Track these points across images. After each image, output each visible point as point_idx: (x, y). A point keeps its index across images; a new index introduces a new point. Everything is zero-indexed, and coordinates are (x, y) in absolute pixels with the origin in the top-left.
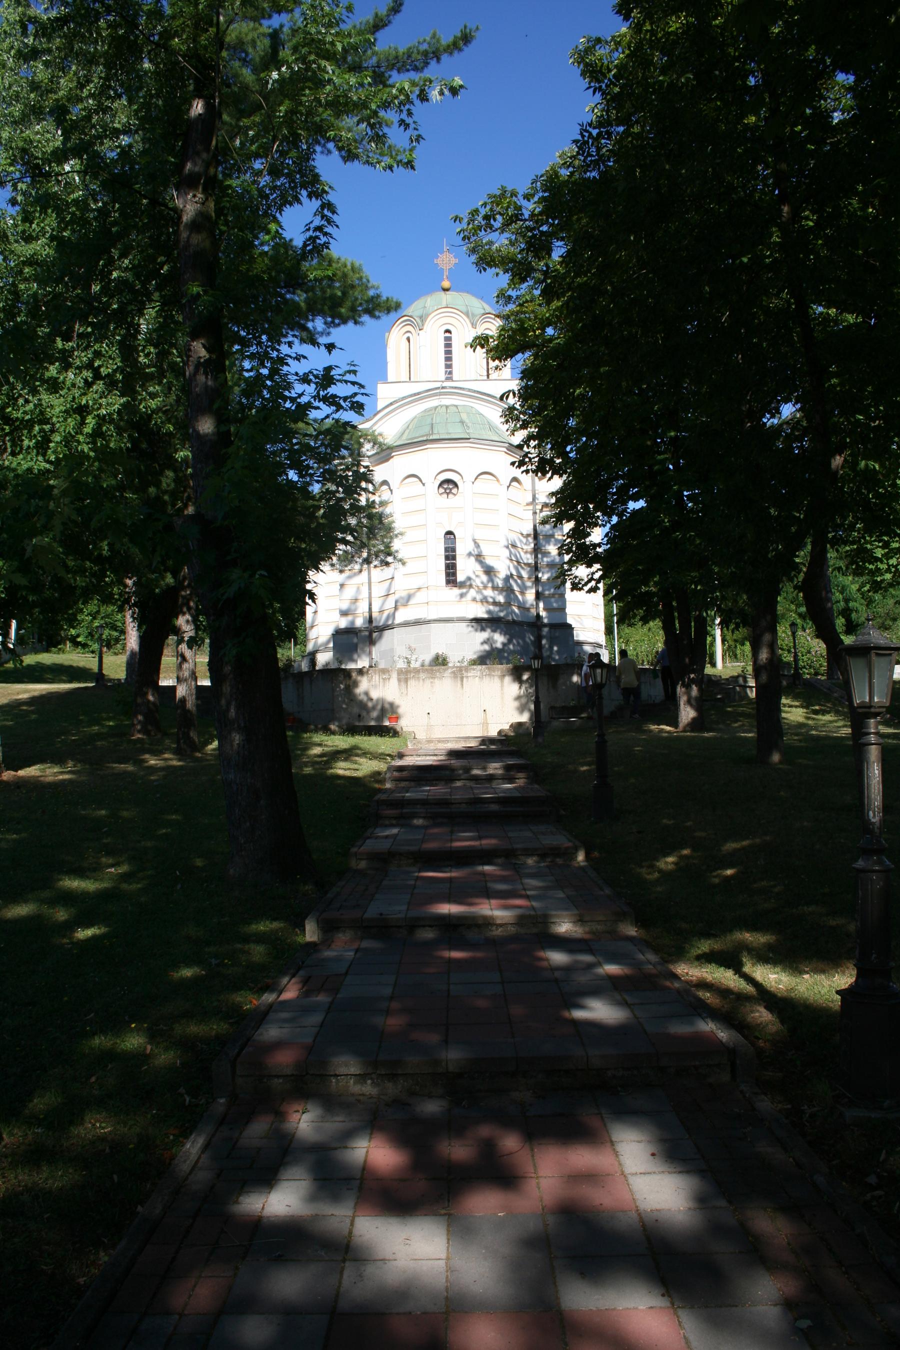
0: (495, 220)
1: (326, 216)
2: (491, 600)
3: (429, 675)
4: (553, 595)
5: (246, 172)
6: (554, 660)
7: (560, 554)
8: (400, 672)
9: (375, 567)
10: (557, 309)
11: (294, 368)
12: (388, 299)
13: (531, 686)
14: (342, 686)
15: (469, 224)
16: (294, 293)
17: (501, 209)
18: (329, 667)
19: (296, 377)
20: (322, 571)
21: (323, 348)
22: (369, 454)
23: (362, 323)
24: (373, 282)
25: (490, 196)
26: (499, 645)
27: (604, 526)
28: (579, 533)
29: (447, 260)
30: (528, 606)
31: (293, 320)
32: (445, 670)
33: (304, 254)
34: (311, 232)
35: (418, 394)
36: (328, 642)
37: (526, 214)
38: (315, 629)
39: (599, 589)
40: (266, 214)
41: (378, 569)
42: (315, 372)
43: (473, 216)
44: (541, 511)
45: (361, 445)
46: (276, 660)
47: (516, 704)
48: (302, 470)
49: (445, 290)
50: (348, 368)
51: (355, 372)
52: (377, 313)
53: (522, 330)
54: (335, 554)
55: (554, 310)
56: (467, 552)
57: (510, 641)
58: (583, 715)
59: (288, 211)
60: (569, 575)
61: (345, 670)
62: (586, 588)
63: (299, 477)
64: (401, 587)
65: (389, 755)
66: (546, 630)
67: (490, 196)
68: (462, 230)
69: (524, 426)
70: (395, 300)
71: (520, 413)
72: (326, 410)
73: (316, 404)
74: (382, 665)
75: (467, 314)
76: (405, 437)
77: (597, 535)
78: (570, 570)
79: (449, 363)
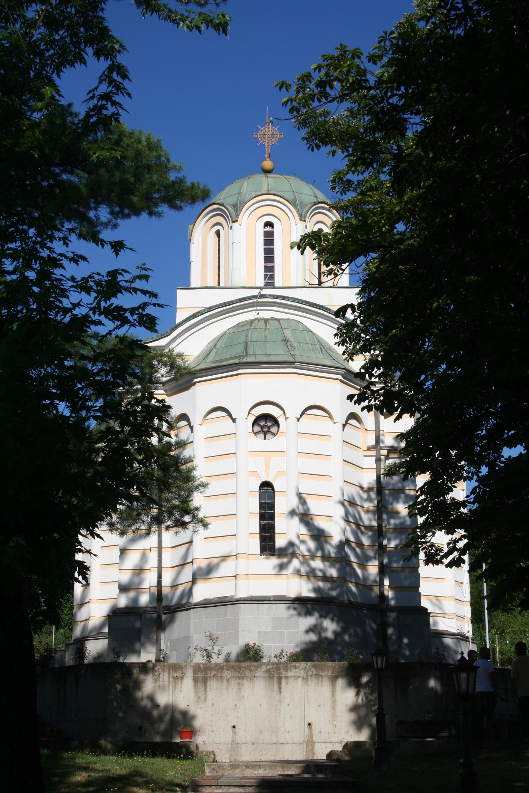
0: (332, 87)
1: (115, 81)
2: (320, 574)
3: (236, 674)
4: (403, 568)
5: (16, 20)
6: (404, 656)
7: (412, 515)
8: (197, 669)
9: (168, 528)
10: (410, 200)
11: (70, 270)
12: (193, 184)
13: (372, 692)
14: (119, 687)
15: (298, 93)
16: (72, 173)
17: (341, 71)
18: (101, 660)
19: (71, 283)
20: (98, 536)
21: (108, 247)
22: (164, 379)
23: (159, 215)
24: (174, 161)
25: (326, 58)
26: (329, 634)
27: (470, 479)
28: (436, 489)
29: (269, 135)
30: (369, 583)
31: (72, 209)
32: (257, 668)
33: (87, 127)
34: (95, 101)
35: (230, 303)
36: (102, 626)
37: (372, 80)
38: (85, 608)
39: (464, 562)
40: (39, 75)
41: (172, 531)
42: (97, 277)
43: (304, 82)
44: (387, 457)
45: (154, 369)
46: (31, 649)
47: (352, 716)
48: (77, 404)
49: (267, 172)
50: (137, 272)
51: (146, 278)
52: (178, 203)
53: (364, 226)
54: (115, 510)
55: (407, 203)
56: (290, 509)
57: (344, 630)
58: (443, 734)
59: (68, 72)
60: (422, 543)
61: (124, 664)
62: (446, 561)
63: (72, 412)
64: (203, 550)
65: (179, 785)
66: (393, 616)
67: (326, 58)
68: (290, 100)
69: (365, 349)
70: (201, 186)
71: (362, 331)
72: (107, 326)
73: (96, 317)
74: (173, 659)
75: (294, 203)
76: (210, 358)
77: (460, 491)
78: (425, 536)
79: (269, 264)
